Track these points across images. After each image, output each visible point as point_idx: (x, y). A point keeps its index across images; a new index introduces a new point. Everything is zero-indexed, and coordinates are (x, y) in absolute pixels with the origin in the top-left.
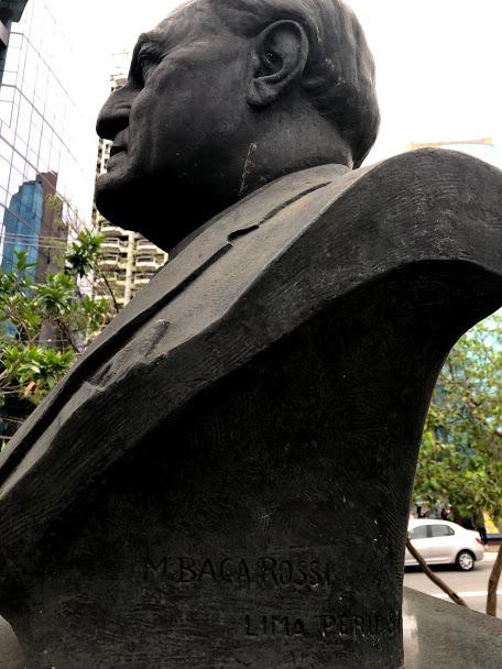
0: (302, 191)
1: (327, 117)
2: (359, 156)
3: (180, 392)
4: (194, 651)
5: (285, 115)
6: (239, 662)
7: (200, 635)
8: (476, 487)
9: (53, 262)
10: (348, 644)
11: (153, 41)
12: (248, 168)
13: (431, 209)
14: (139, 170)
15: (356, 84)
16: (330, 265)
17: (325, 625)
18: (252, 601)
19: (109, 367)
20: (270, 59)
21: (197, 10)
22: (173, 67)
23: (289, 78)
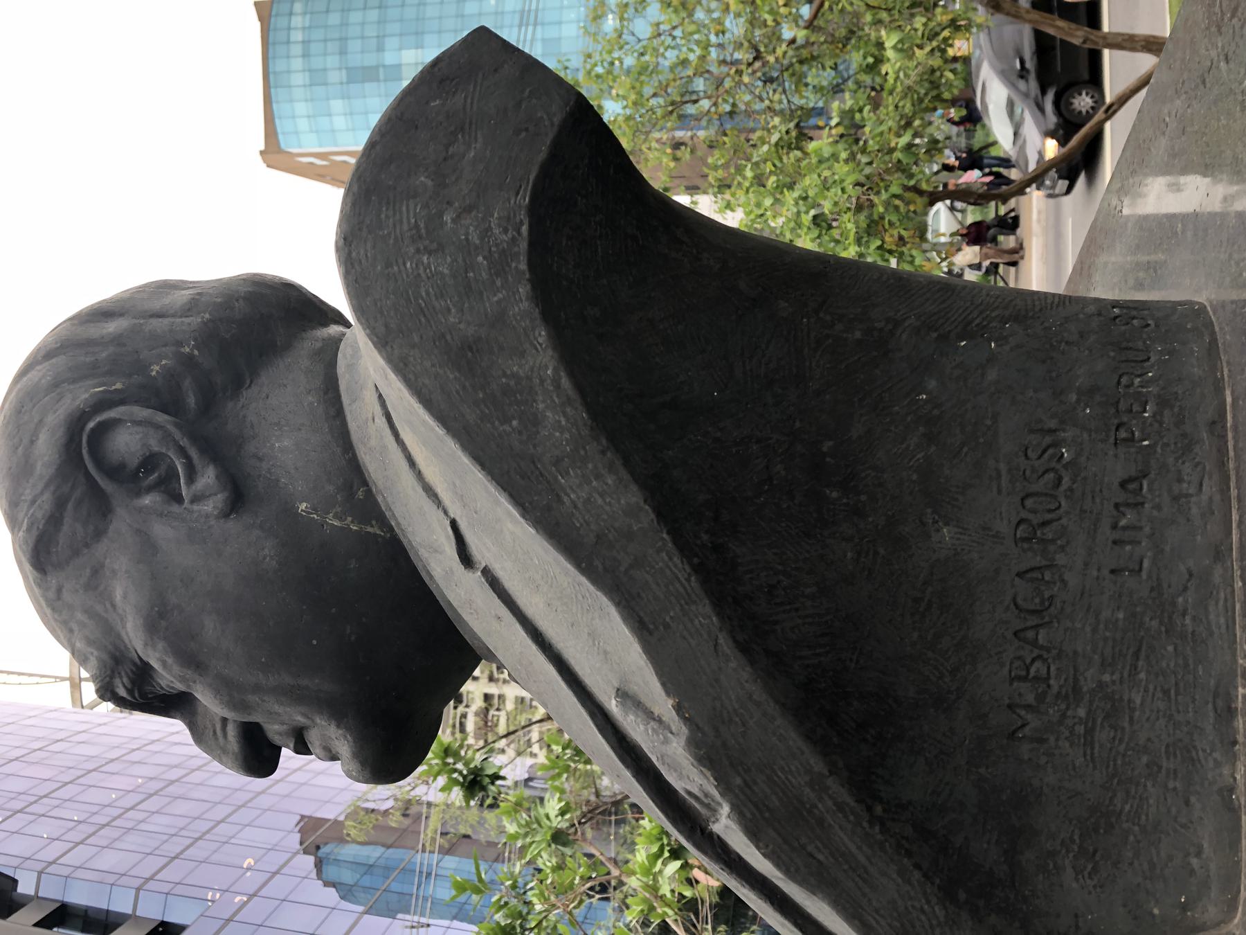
0: (388, 431)
1: (254, 374)
2: (329, 315)
3: (737, 679)
4: (1164, 664)
5: (251, 448)
6: (1185, 589)
7: (1139, 650)
8: (912, 64)
9: (469, 832)
10: (1164, 402)
11: (112, 677)
12: (340, 519)
13: (441, 248)
14: (337, 711)
15: (195, 321)
16: (534, 421)
17: (1131, 439)
18: (1086, 565)
19: (689, 793)
20: (150, 474)
21: (59, 598)
22: (161, 645)
23: (184, 442)
